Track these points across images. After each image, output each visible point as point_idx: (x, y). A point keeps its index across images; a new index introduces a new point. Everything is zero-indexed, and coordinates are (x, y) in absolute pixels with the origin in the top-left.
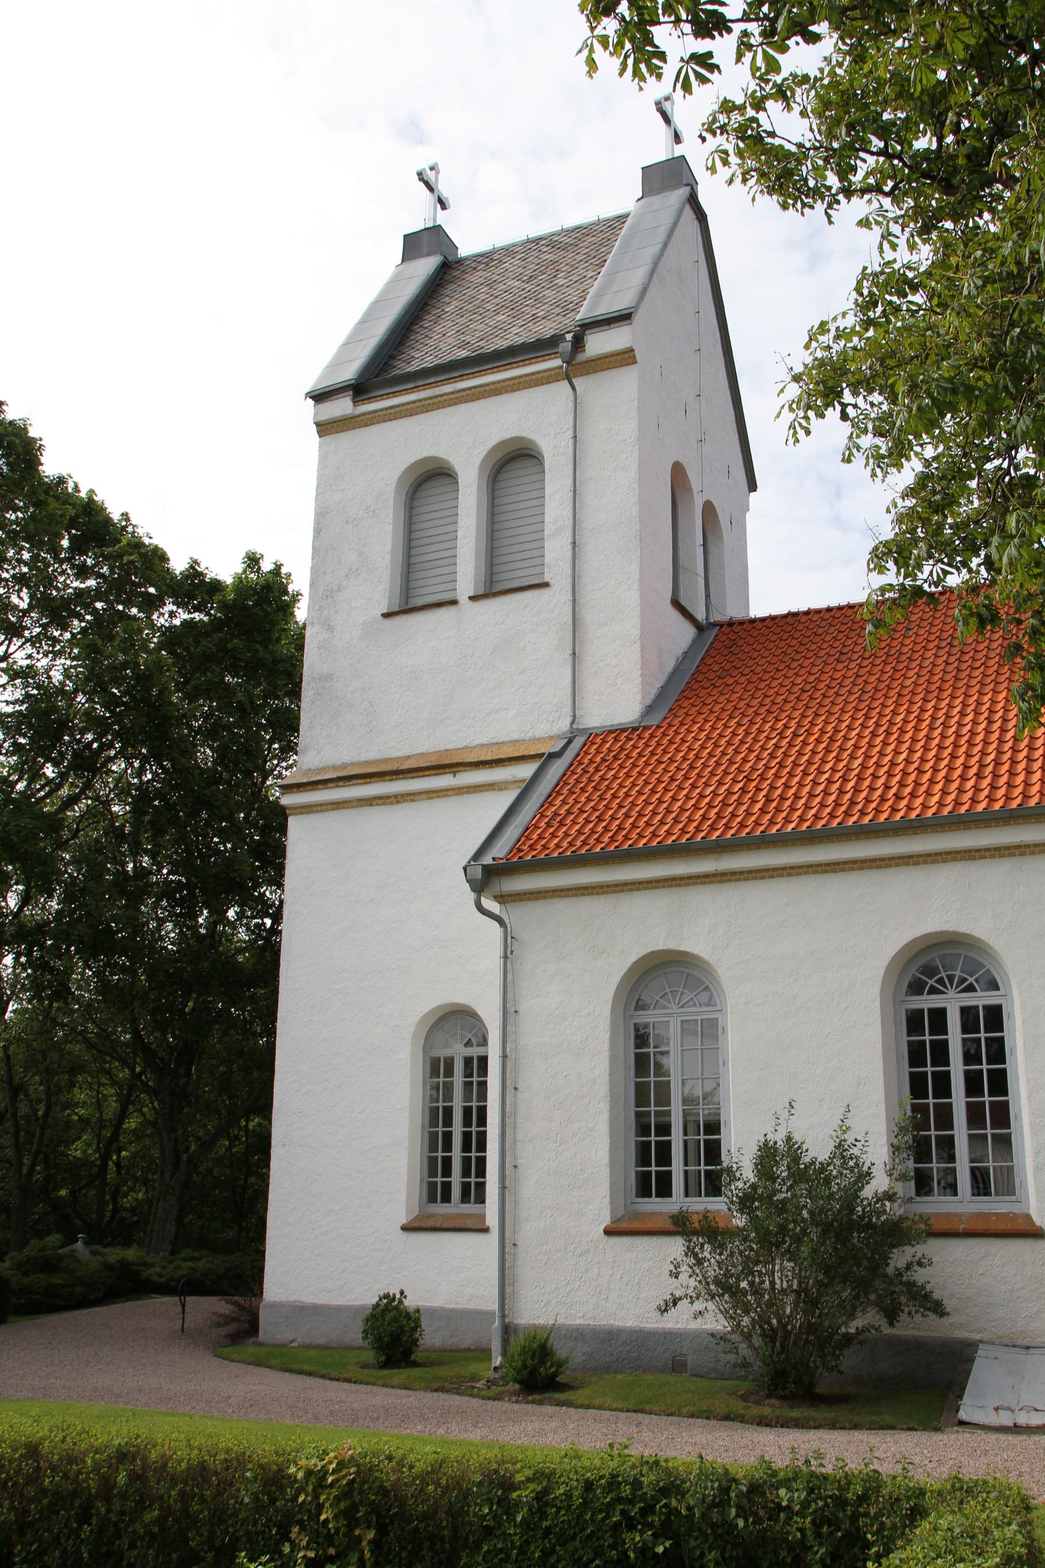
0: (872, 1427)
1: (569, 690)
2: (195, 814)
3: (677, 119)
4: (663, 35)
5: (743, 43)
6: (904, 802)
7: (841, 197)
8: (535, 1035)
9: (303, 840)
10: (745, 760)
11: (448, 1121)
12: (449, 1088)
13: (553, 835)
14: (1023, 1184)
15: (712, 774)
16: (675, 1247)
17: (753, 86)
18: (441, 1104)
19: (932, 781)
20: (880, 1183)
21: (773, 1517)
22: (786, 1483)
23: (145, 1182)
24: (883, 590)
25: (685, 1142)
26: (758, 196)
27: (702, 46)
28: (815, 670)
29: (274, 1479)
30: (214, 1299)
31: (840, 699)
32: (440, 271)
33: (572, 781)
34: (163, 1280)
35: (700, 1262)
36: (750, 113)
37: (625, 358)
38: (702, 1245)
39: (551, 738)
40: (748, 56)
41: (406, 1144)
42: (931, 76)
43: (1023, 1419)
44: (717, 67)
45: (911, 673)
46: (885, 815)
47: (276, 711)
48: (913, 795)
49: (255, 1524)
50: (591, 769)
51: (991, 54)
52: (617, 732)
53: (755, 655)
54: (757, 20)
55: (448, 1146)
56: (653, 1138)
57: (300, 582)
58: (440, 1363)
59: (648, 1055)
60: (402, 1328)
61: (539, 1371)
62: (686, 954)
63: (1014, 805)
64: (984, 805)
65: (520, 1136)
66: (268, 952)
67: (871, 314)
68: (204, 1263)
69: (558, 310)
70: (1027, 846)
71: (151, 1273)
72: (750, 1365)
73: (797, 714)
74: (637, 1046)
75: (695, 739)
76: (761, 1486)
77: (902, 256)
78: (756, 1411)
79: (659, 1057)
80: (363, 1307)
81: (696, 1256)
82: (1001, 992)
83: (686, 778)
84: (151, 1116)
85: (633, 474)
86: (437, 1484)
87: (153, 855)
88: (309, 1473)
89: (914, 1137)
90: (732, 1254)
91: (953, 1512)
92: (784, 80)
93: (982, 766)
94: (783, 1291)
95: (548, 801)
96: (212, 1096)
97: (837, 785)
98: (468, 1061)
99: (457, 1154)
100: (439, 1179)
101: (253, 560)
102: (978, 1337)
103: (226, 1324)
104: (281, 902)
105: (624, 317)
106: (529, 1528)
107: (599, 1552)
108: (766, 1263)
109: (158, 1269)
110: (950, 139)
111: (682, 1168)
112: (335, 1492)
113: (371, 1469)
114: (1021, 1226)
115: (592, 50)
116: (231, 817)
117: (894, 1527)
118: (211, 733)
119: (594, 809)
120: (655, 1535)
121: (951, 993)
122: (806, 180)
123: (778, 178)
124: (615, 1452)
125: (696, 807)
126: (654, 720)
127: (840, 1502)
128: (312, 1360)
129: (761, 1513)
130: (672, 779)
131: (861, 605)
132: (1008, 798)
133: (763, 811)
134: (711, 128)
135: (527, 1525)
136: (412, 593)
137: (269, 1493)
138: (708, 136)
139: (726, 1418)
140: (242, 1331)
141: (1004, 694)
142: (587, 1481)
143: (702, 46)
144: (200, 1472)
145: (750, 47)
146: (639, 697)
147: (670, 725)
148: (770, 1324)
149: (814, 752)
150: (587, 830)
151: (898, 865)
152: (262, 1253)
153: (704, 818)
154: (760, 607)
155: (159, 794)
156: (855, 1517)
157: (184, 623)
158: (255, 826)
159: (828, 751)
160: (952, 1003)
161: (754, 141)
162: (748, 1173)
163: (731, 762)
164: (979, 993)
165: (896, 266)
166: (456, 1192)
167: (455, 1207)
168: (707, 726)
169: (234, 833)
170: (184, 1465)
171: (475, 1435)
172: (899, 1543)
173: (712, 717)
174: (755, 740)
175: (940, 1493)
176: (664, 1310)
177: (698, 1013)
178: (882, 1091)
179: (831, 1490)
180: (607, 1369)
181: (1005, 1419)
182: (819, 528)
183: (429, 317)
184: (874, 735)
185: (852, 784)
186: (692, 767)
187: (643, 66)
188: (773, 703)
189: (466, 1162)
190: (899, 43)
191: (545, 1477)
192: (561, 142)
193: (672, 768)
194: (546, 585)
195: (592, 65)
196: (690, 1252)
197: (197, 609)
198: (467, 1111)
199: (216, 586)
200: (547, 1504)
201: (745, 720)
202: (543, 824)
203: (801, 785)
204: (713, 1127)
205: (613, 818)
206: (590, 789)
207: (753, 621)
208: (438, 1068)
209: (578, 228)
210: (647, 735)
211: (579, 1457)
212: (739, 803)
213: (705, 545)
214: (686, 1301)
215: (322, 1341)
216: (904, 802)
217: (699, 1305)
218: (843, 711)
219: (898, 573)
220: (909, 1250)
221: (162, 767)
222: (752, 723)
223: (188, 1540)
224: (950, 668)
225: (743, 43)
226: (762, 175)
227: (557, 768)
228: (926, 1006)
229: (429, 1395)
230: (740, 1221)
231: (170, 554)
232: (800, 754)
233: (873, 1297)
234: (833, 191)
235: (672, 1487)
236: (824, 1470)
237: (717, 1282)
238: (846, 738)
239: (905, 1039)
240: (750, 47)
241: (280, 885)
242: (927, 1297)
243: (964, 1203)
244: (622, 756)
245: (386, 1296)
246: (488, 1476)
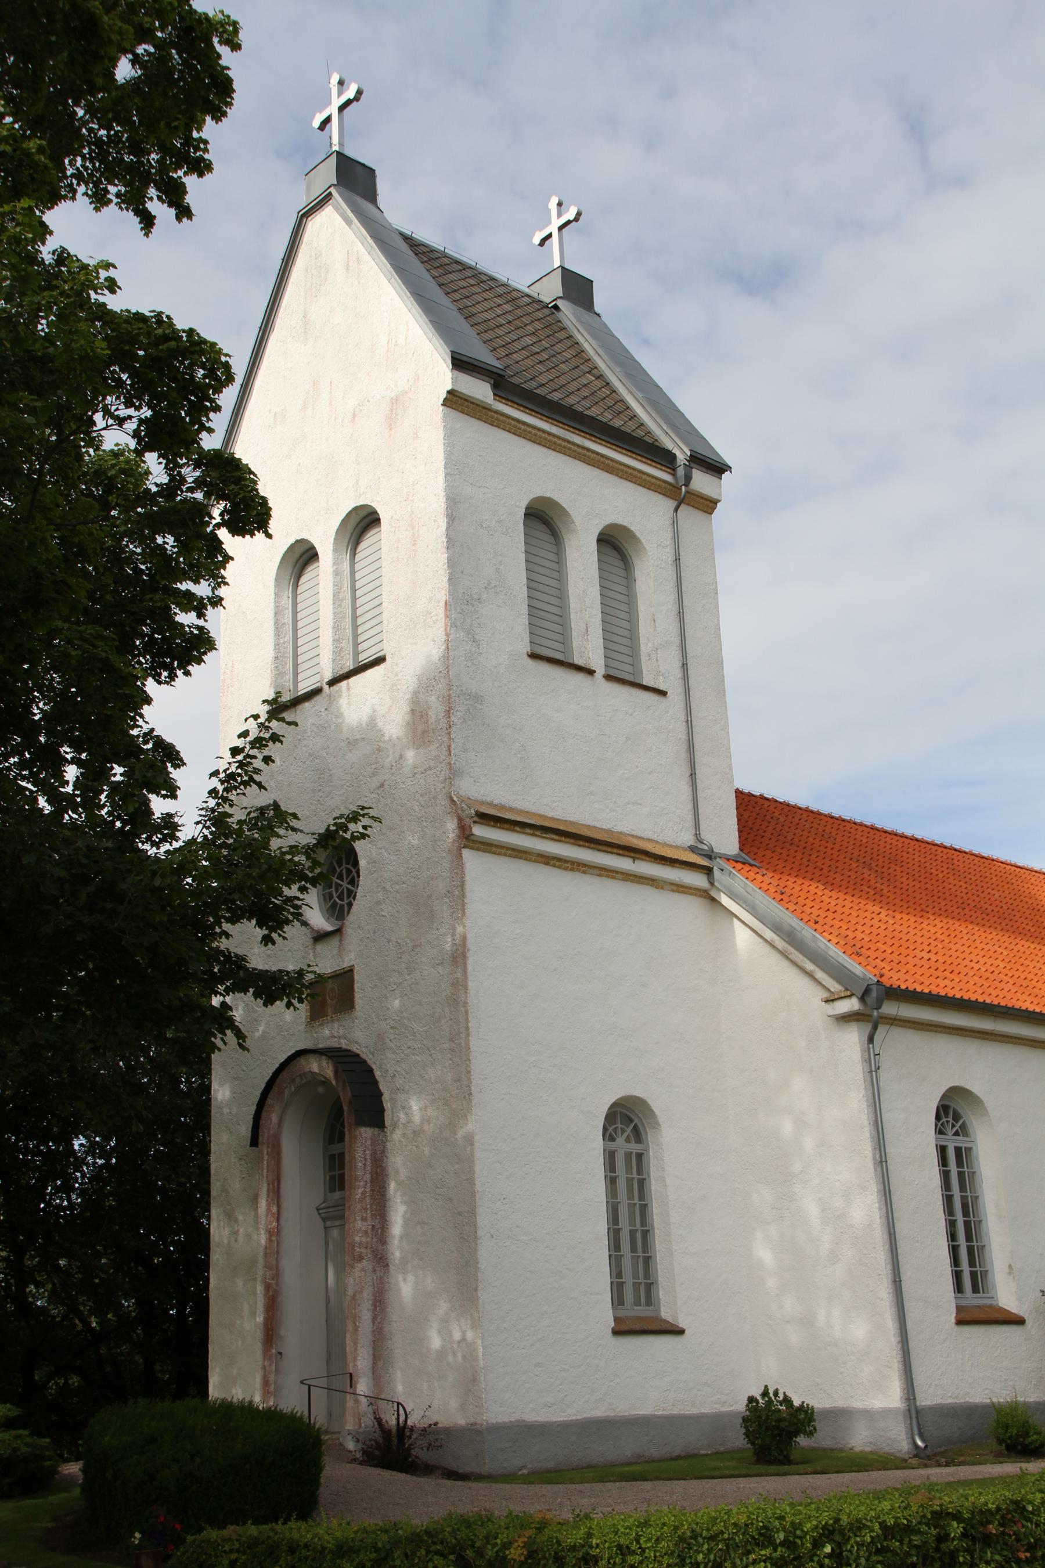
98: (628, 1156)
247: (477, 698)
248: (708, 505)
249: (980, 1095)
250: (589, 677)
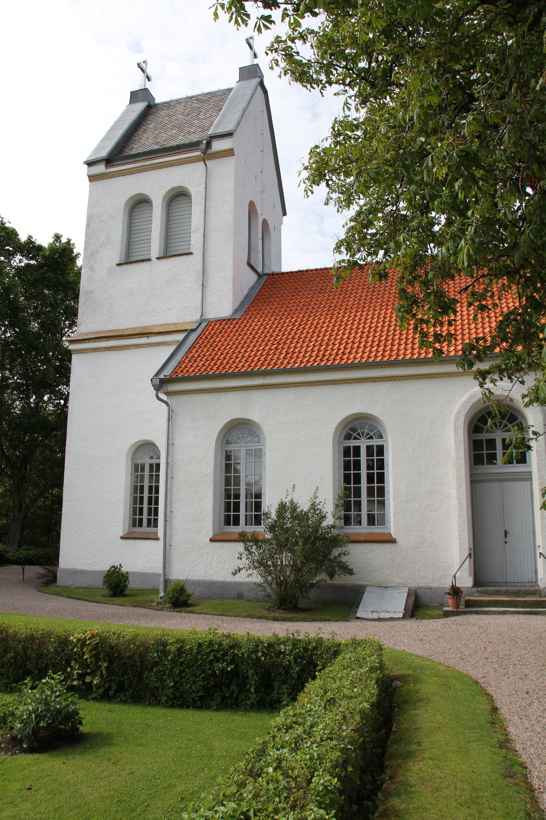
0: (321, 620)
1: (200, 301)
2: (29, 352)
3: (255, 47)
4: (249, 6)
5: (285, 14)
6: (346, 356)
7: (327, 85)
8: (181, 454)
9: (79, 366)
10: (277, 335)
11: (142, 491)
12: (142, 477)
13: (191, 366)
14: (389, 521)
15: (263, 341)
16: (240, 547)
17: (290, 32)
18: (139, 484)
19: (358, 347)
20: (329, 521)
21: (277, 656)
22: (284, 643)
23: (6, 516)
24: (340, 262)
25: (246, 502)
26: (291, 82)
27: (267, 12)
28: (310, 296)
29: (64, 642)
30: (37, 567)
31: (320, 310)
32: (147, 109)
33: (200, 342)
35: (251, 553)
36: (289, 43)
37: (229, 153)
38: (252, 546)
39: (192, 322)
40: (287, 19)
41: (123, 501)
42: (366, 36)
43: (382, 615)
44: (274, 22)
45: (351, 300)
46: (338, 361)
47: (67, 307)
48: (350, 353)
49: (55, 659)
50: (209, 337)
51: (391, 30)
52: (221, 321)
53: (283, 288)
54: (291, 4)
55: (141, 502)
56: (232, 500)
57: (79, 248)
58: (137, 595)
59: (231, 464)
60: (120, 581)
61: (180, 599)
62: (249, 420)
63: (393, 358)
64: (380, 358)
66: (62, 414)
67: (338, 139)
68: (33, 552)
69: (200, 130)
70: (398, 377)
71: (9, 555)
72: (271, 596)
73: (301, 315)
74: (226, 460)
75: (256, 325)
76: (273, 644)
77: (353, 115)
78: (272, 615)
79: (236, 465)
80: (103, 571)
81: (249, 550)
83: (251, 342)
84: (9, 487)
85: (232, 205)
86: (135, 645)
87: (11, 370)
88: (79, 640)
89: (345, 501)
90: (265, 550)
91: (351, 652)
92: (303, 31)
93: (380, 341)
94: (286, 565)
95: (190, 351)
96: (37, 479)
97: (317, 347)
98: (151, 466)
99: (145, 506)
100: (138, 517)
101: (57, 237)
102: (366, 584)
103: (43, 577)
104: (68, 393)
105: (229, 135)
106: (174, 662)
107: (203, 671)
108: (279, 554)
109: (12, 554)
110: (374, 64)
111: (244, 513)
112: (90, 647)
113: (106, 638)
114: (387, 538)
115: (217, 9)
116: (46, 355)
117: (327, 659)
118: (37, 316)
119: (210, 355)
120: (227, 664)
121: (363, 439)
122: (312, 76)
123: (300, 75)
124: (212, 631)
125: (255, 355)
126: (238, 316)
127: (306, 649)
128: (81, 593)
129: (273, 655)
130: (245, 343)
131: (331, 269)
132: (390, 356)
133: (285, 358)
134: (272, 49)
135: (173, 661)
136: (130, 255)
137: (61, 647)
138: (269, 52)
139: (260, 618)
140: (50, 580)
141: (390, 310)
142: (199, 643)
143: (267, 12)
144: (31, 638)
145: (288, 15)
146: (231, 305)
147: (245, 319)
148: (280, 579)
149: (308, 333)
150: (206, 364)
151: (342, 383)
152: (58, 548)
153: (259, 360)
154: (285, 268)
155: (13, 342)
156: (311, 655)
157: (28, 265)
158: (58, 359)
159: (314, 332)
161: (289, 56)
162: (274, 516)
163: (271, 336)
164: (375, 440)
165: (350, 119)
166: (145, 522)
167: (145, 529)
168: (261, 320)
169: (47, 361)
170: (24, 635)
171: (152, 625)
172: (329, 665)
173: (264, 316)
174: (282, 326)
175: (347, 645)
176: (234, 574)
177: (254, 446)
178: (332, 481)
179: (301, 645)
180: (210, 598)
181: (375, 616)
182: (313, 234)
183: (141, 130)
184: (334, 326)
185: (324, 347)
186: (254, 338)
187: (239, 19)
188: (291, 310)
189: (150, 510)
190: (353, 20)
191: (182, 642)
192: (202, 56)
193: (245, 338)
194: (191, 253)
195: (216, 15)
196: (246, 549)
197: (32, 259)
198: (150, 488)
199: (40, 248)
200: (182, 652)
201: (278, 317)
202: (187, 361)
203: (302, 347)
204: (258, 496)
205: (218, 359)
206: (208, 346)
207: (283, 274)
208: (138, 468)
209: (210, 93)
210: (234, 323)
211: (196, 634)
212: (274, 354)
213: (263, 239)
214: (244, 570)
215: (85, 585)
216: (346, 356)
217: (250, 572)
218: (321, 315)
219: (347, 254)
220: (340, 549)
221: (15, 331)
222: (281, 319)
223: (26, 665)
224: (368, 298)
225: (285, 14)
226: (293, 73)
227: (193, 337)
229: (132, 608)
230: (269, 536)
231: (19, 232)
232: (302, 333)
233: (324, 568)
234: (323, 82)
235: (236, 645)
236: (300, 638)
237: (258, 562)
238: (322, 327)
239: (342, 459)
240: (288, 15)
241: (68, 385)
242: (346, 568)
243: (364, 529)
244: (223, 331)
245: (114, 567)
246: (157, 641)
249: (257, 420)
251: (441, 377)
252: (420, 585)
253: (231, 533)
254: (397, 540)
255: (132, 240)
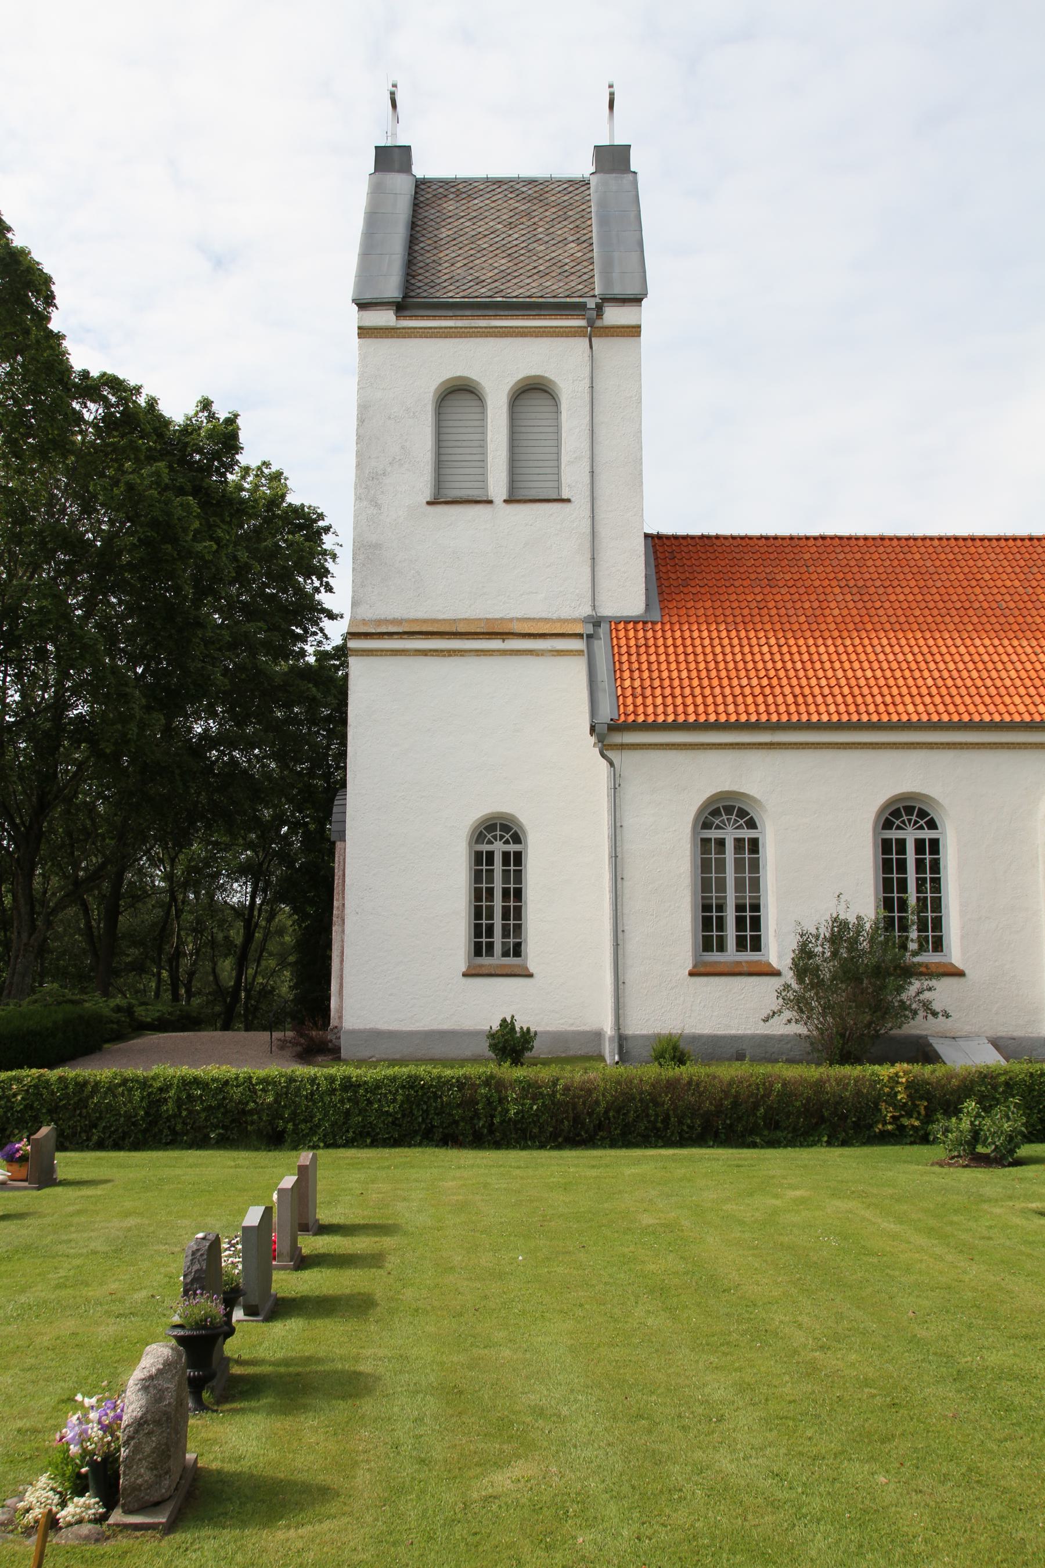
34: (149, 1020)
65: (626, 911)
82: (939, 831)
101: (206, 405)
121: (910, 829)
160: (910, 835)
166: (498, 949)
176: (766, 1020)
208: (481, 861)
228: (894, 837)
247: (377, 546)
248: (634, 331)
249: (757, 796)
250: (489, 506)
251: (1026, 748)
252: (1000, 1034)
253: (716, 963)
254: (967, 972)
255: (443, 458)
